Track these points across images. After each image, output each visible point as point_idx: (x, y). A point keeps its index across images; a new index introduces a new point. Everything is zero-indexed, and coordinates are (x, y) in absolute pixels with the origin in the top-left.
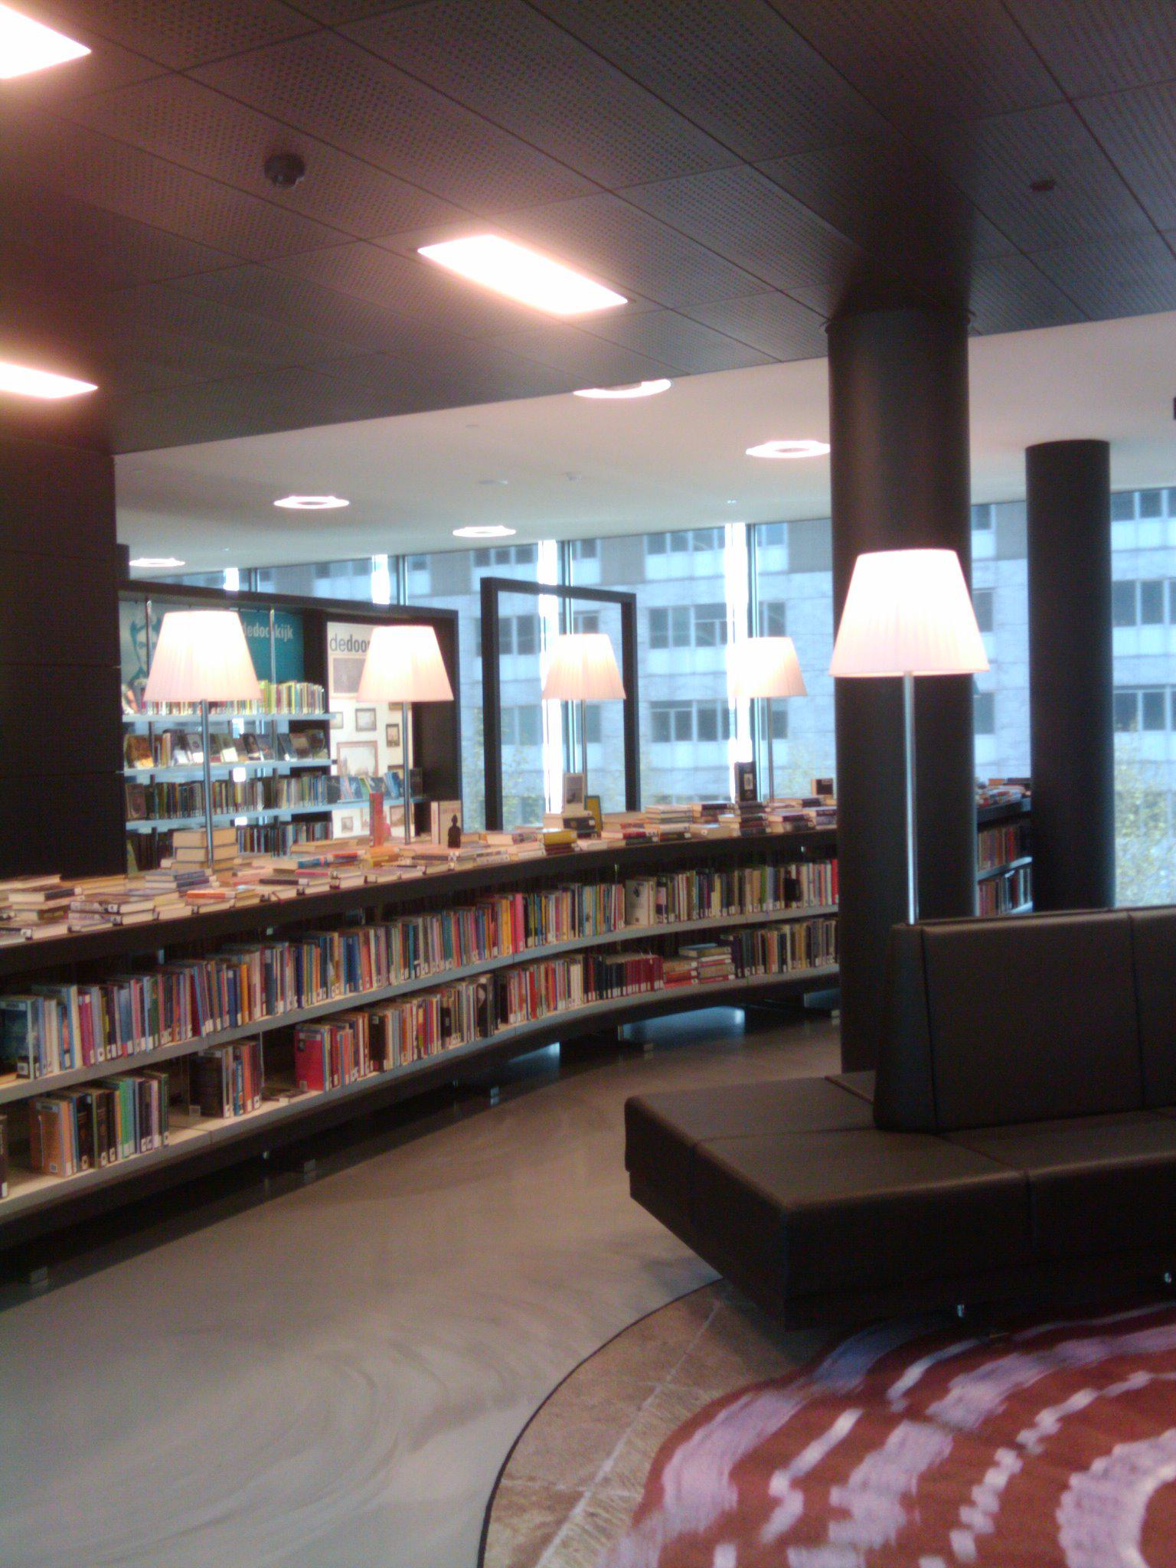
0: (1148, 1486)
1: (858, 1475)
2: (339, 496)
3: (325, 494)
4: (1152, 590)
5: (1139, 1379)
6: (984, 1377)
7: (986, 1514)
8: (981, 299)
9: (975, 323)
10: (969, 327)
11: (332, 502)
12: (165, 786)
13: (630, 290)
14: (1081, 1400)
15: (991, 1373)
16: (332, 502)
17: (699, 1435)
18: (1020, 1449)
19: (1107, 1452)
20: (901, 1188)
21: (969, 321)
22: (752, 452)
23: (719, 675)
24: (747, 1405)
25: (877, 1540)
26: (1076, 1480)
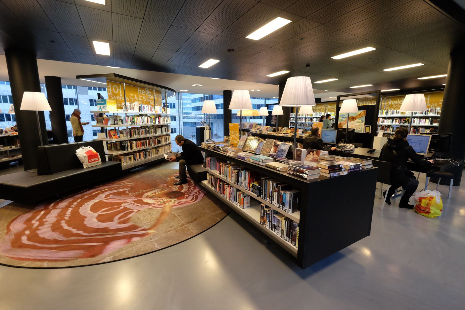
0: (91, 205)
1: (47, 217)
2: (187, 90)
3: (186, 90)
4: (5, 101)
5: (87, 197)
6: (64, 202)
7: (69, 214)
8: (39, 54)
9: (37, 57)
10: (37, 57)
11: (187, 91)
12: (7, 145)
13: (212, 56)
14: (79, 200)
15: (65, 201)
16: (187, 91)
17: (14, 222)
18: (72, 207)
19: (84, 204)
20: (35, 184)
21: (36, 56)
22: (193, 85)
23: (123, 117)
24: (22, 216)
25: (53, 222)
26: (81, 208)
